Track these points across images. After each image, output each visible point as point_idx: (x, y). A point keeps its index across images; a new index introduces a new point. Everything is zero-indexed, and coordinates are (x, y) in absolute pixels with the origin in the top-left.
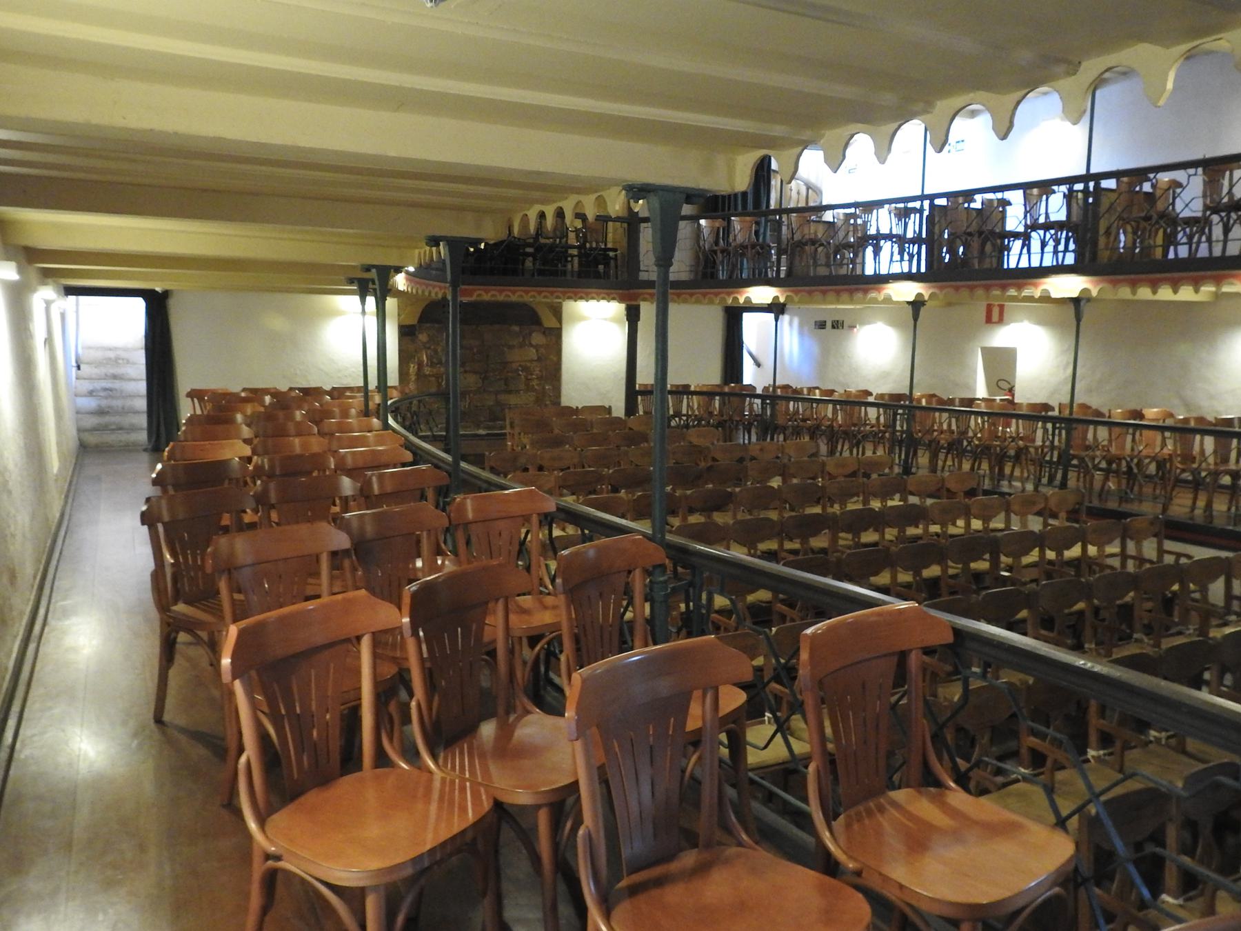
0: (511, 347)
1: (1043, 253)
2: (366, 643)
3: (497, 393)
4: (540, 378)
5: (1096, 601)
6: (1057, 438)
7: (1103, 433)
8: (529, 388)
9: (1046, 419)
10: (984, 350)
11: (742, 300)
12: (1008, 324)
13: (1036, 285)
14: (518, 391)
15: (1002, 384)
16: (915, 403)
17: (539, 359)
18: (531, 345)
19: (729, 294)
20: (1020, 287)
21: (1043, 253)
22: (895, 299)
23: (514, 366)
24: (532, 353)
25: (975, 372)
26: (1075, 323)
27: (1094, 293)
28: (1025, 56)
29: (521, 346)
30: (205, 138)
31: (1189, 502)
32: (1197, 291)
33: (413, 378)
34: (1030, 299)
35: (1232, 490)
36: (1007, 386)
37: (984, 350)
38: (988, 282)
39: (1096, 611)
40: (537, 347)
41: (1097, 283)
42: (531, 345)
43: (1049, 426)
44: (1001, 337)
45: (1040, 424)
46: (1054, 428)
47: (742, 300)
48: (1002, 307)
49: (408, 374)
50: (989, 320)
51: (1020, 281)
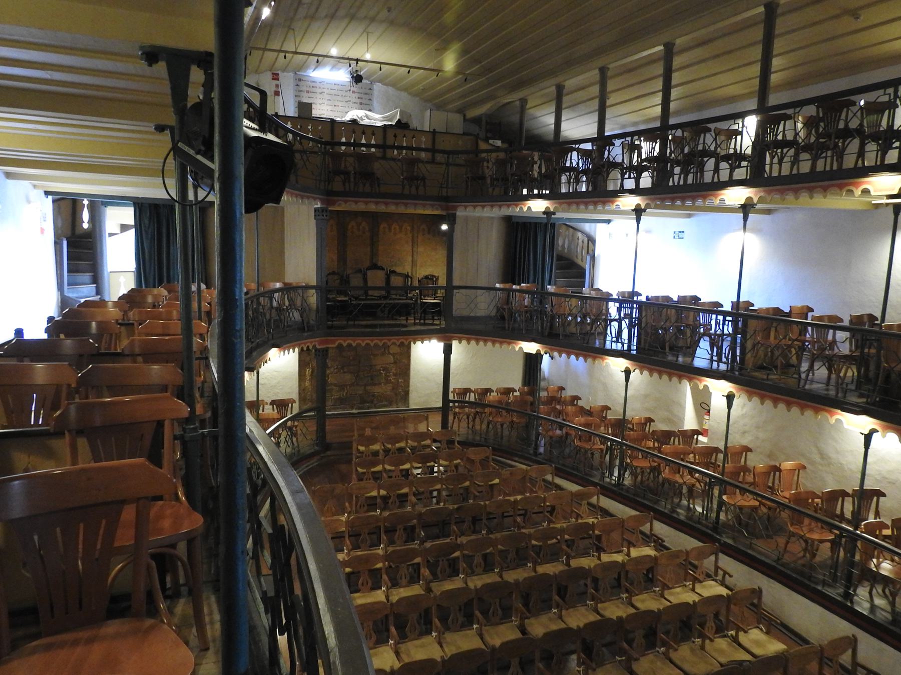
0: (375, 355)
2: (268, 432)
3: (365, 385)
4: (395, 375)
6: (726, 327)
8: (388, 381)
9: (718, 313)
11: (525, 209)
14: (380, 384)
17: (395, 362)
18: (389, 353)
19: (517, 206)
20: (704, 198)
23: (378, 367)
24: (391, 359)
28: (758, 148)
29: (383, 354)
30: (198, 52)
33: (308, 378)
35: (897, 541)
40: (393, 355)
42: (389, 353)
43: (720, 318)
45: (714, 316)
46: (724, 320)
49: (305, 375)
51: (705, 193)
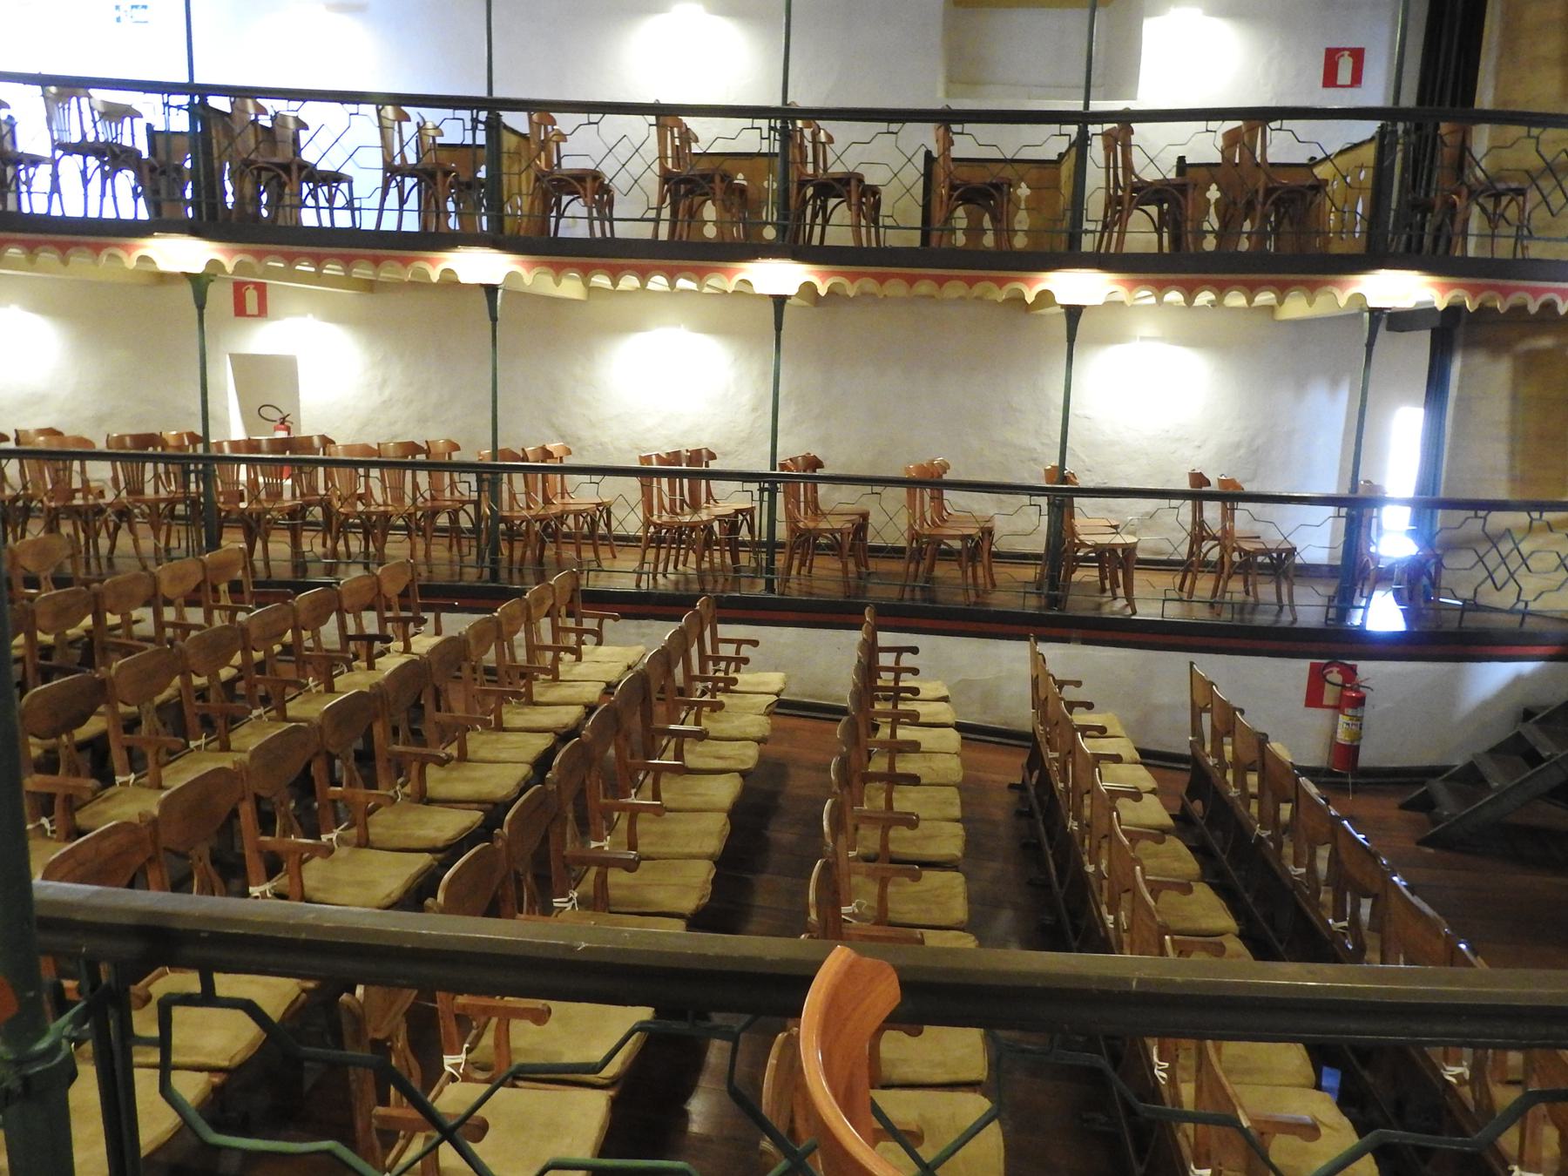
1: (401, 210)
3: (477, 504)
5: (122, 708)
7: (100, 472)
10: (235, 358)
12: (275, 318)
13: (729, 274)
15: (266, 412)
16: (214, 452)
21: (401, 210)
22: (463, 279)
25: (226, 398)
26: (195, 311)
27: (1470, 306)
31: (1211, 585)
32: (1310, 303)
34: (421, 285)
36: (277, 416)
37: (235, 358)
38: (379, 252)
39: (131, 724)
41: (824, 276)
44: (262, 339)
47: (435, 276)
48: (261, 289)
50: (240, 310)
